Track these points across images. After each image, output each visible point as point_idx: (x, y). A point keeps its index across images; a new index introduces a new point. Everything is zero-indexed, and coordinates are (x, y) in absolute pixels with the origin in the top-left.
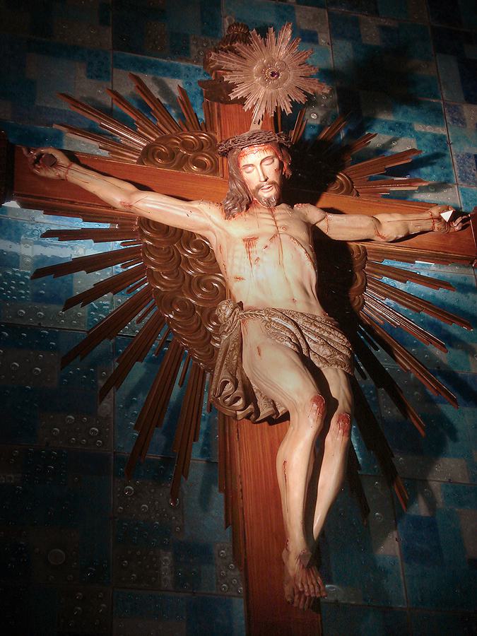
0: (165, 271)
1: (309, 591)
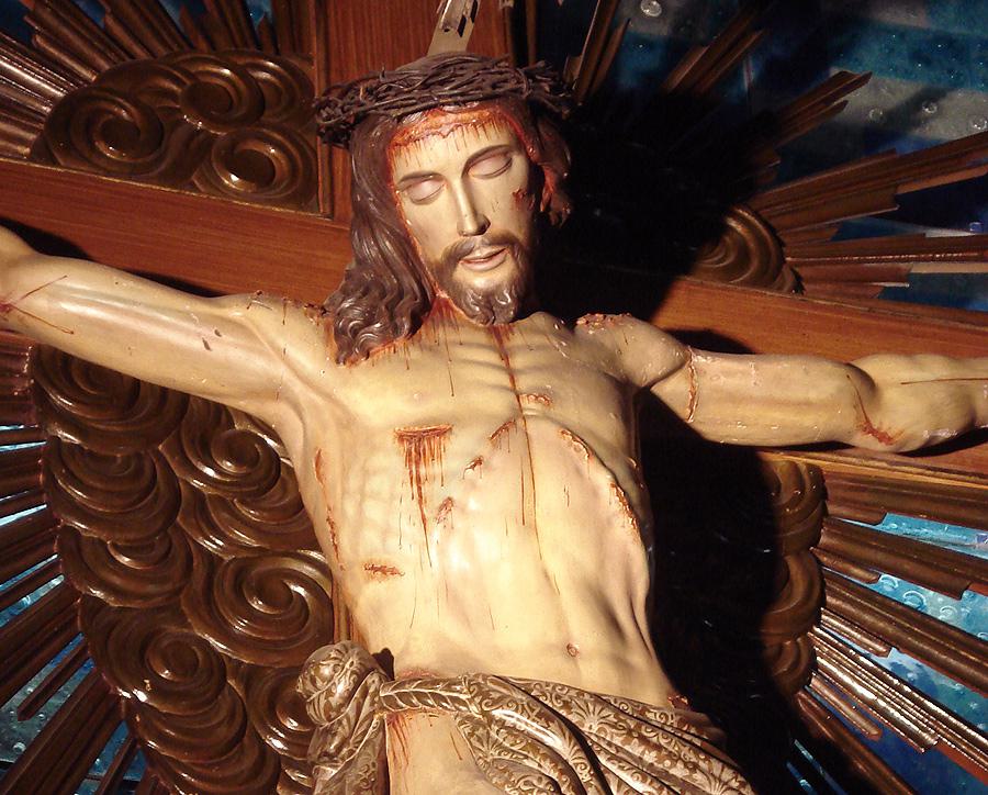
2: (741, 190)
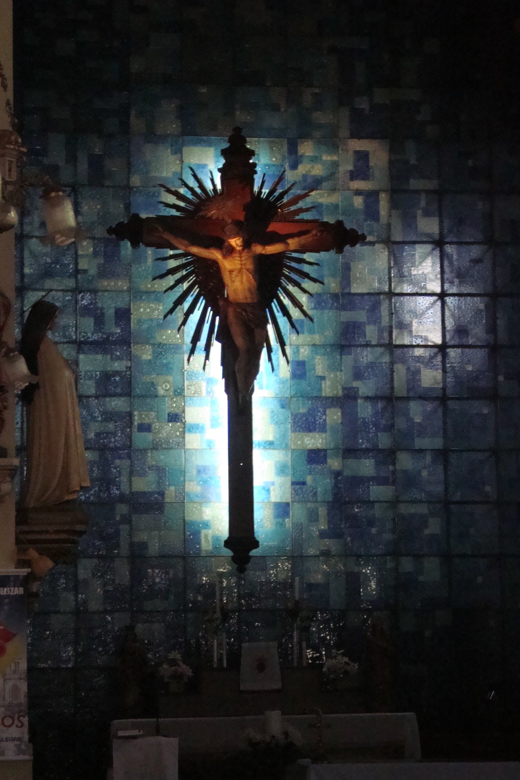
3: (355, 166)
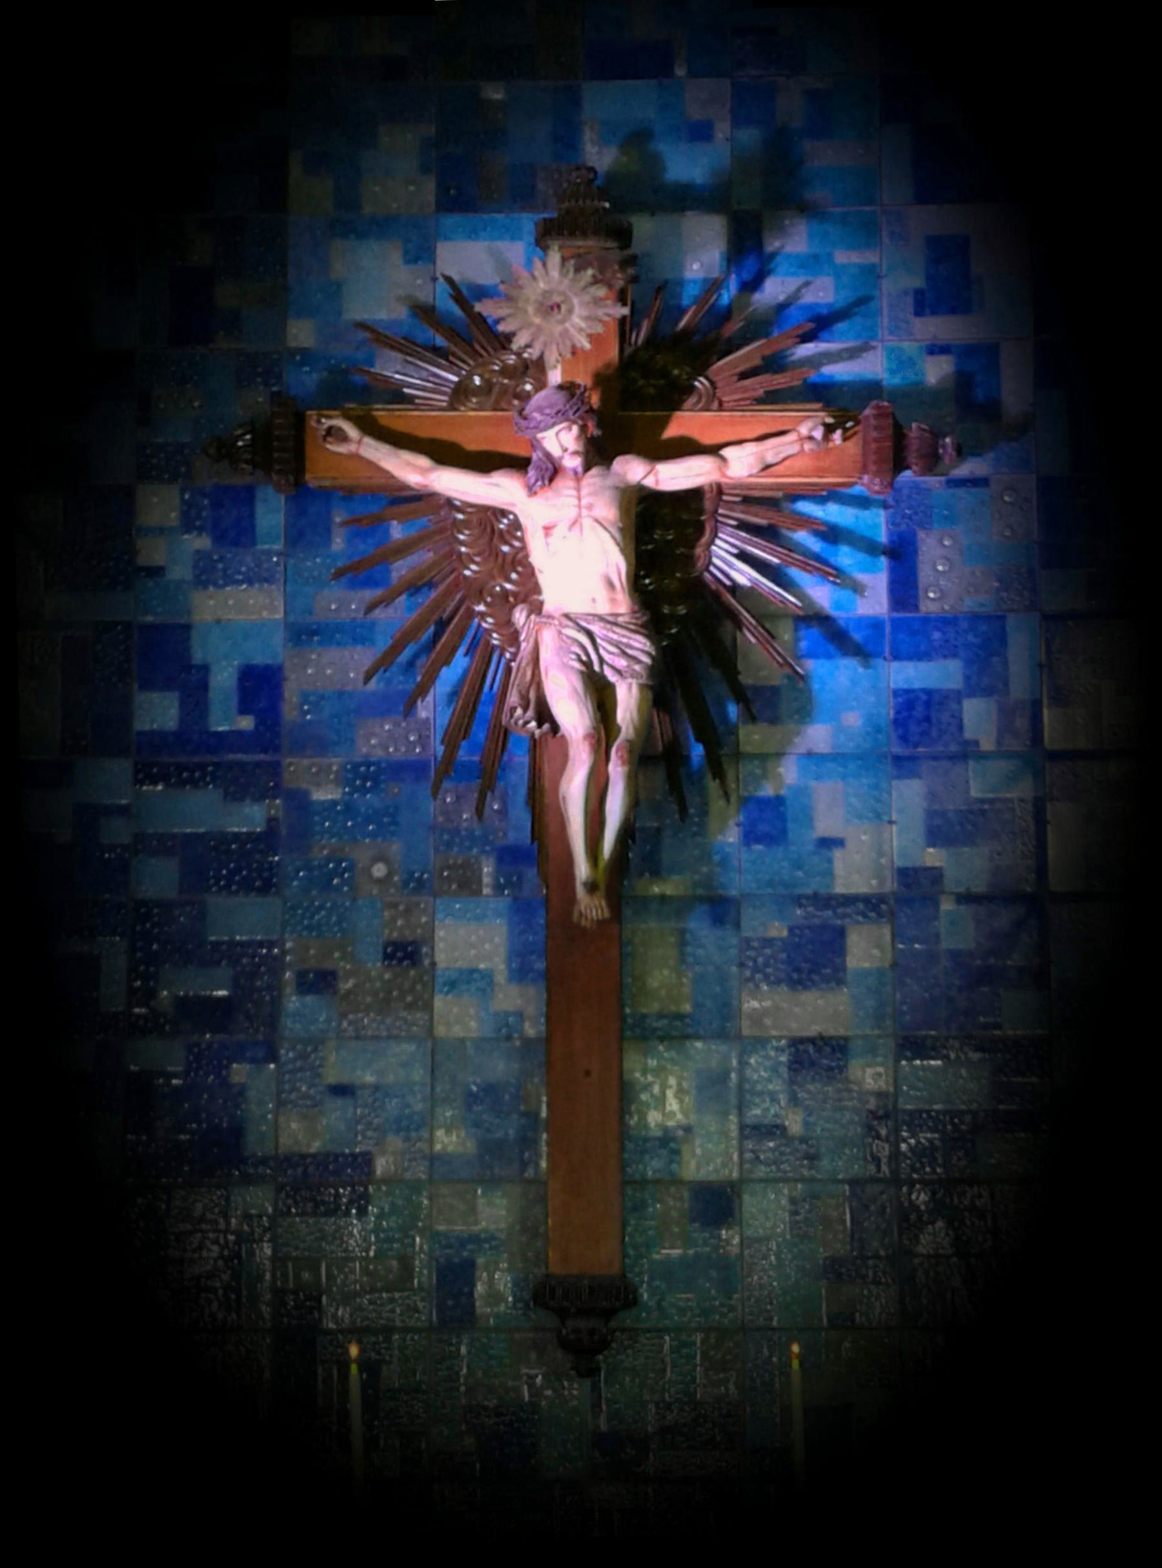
0: (476, 550)
1: (597, 915)
2: (701, 369)
3: (929, 278)
